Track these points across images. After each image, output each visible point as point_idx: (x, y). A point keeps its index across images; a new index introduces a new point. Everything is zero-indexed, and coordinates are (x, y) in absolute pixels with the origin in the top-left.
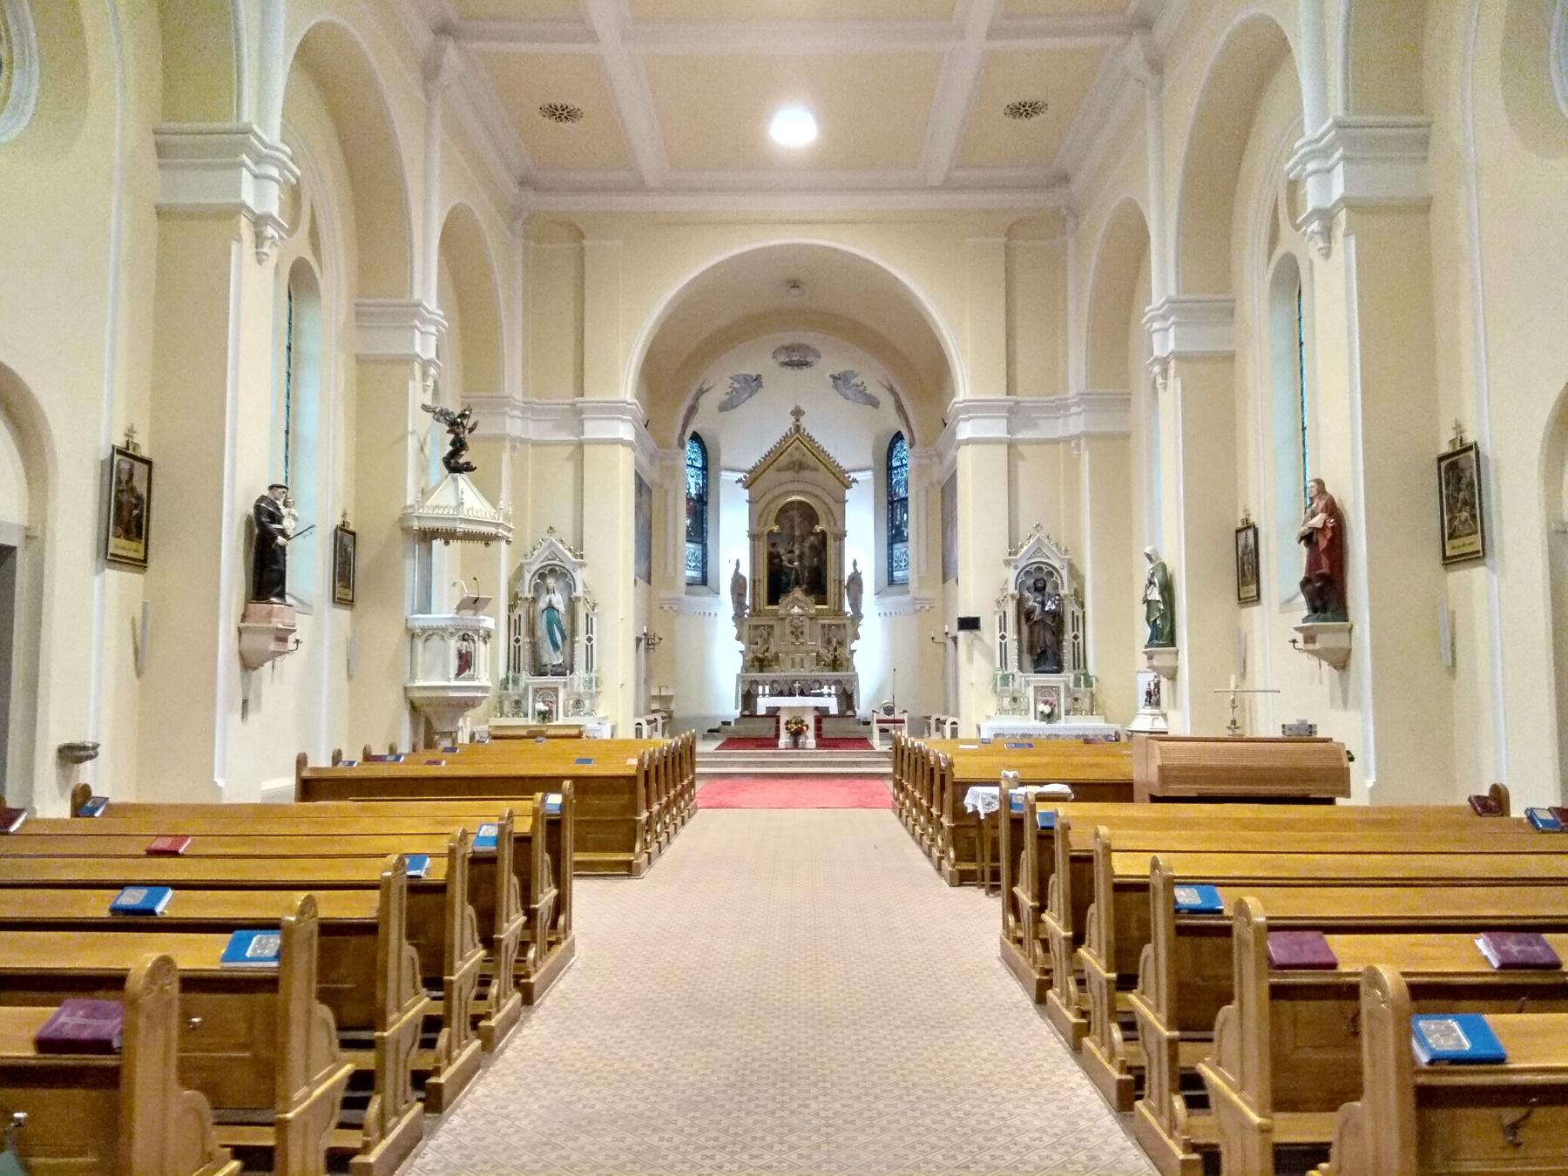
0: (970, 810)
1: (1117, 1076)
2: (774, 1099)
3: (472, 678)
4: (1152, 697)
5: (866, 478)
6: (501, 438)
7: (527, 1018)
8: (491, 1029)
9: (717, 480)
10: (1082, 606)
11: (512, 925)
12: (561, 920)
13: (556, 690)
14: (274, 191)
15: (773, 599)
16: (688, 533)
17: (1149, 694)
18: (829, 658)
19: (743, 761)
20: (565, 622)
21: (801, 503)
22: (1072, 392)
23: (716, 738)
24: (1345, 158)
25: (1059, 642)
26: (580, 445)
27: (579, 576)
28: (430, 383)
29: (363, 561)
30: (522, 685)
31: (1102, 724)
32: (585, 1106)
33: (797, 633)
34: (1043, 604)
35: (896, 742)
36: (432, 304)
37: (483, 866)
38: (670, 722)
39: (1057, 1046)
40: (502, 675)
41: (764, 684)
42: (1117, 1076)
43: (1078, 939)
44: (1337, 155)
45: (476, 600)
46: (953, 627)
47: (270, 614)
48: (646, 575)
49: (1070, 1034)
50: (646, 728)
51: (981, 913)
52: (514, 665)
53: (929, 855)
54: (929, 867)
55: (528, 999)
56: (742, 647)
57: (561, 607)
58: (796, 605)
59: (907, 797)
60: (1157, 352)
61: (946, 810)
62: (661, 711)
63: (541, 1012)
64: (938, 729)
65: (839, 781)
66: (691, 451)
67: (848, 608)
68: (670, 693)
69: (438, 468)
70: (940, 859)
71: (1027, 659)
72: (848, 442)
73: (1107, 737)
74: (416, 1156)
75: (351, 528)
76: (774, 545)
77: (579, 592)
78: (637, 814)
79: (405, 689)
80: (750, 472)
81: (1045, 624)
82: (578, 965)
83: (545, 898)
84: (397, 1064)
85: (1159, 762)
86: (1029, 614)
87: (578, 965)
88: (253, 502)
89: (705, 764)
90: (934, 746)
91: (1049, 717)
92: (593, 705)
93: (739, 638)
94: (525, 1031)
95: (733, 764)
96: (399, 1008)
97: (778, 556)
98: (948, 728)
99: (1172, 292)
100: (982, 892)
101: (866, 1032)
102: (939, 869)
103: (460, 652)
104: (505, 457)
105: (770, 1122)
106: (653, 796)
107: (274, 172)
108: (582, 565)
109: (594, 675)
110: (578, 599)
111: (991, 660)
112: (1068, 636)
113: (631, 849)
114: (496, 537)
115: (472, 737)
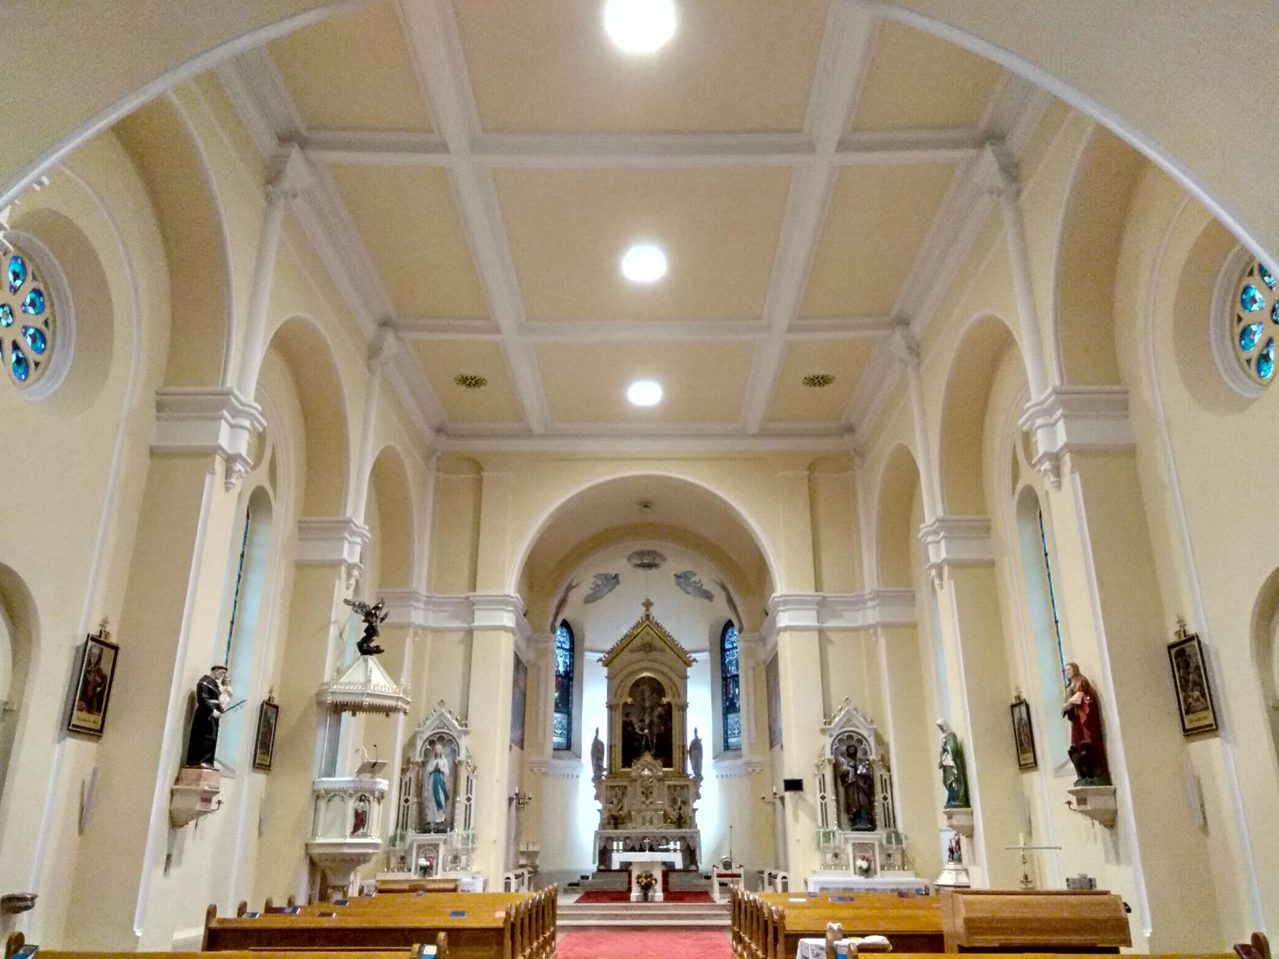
3: (365, 835)
5: (703, 657)
6: (404, 627)
10: (889, 770)
13: (436, 846)
15: (627, 762)
16: (557, 705)
17: (951, 851)
18: (674, 815)
19: (598, 914)
20: (449, 786)
21: (650, 678)
26: (470, 632)
27: (464, 743)
28: (353, 582)
30: (408, 842)
33: (647, 793)
34: (855, 768)
35: (734, 894)
36: (360, 520)
38: (535, 877)
40: (391, 832)
41: (618, 840)
47: (199, 778)
48: (520, 742)
50: (513, 882)
52: (402, 824)
58: (647, 767)
60: (933, 559)
66: (561, 636)
67: (690, 771)
68: (535, 848)
69: (353, 650)
71: (845, 818)
72: (689, 627)
73: (918, 891)
76: (628, 715)
77: (462, 756)
80: (609, 653)
81: (858, 787)
86: (844, 776)
90: (767, 898)
91: (866, 872)
92: (468, 861)
93: (597, 798)
97: (631, 724)
98: (779, 881)
104: (409, 641)
106: (518, 948)
107: (247, 423)
108: (466, 733)
109: (470, 832)
110: (460, 762)
111: (815, 820)
112: (879, 797)
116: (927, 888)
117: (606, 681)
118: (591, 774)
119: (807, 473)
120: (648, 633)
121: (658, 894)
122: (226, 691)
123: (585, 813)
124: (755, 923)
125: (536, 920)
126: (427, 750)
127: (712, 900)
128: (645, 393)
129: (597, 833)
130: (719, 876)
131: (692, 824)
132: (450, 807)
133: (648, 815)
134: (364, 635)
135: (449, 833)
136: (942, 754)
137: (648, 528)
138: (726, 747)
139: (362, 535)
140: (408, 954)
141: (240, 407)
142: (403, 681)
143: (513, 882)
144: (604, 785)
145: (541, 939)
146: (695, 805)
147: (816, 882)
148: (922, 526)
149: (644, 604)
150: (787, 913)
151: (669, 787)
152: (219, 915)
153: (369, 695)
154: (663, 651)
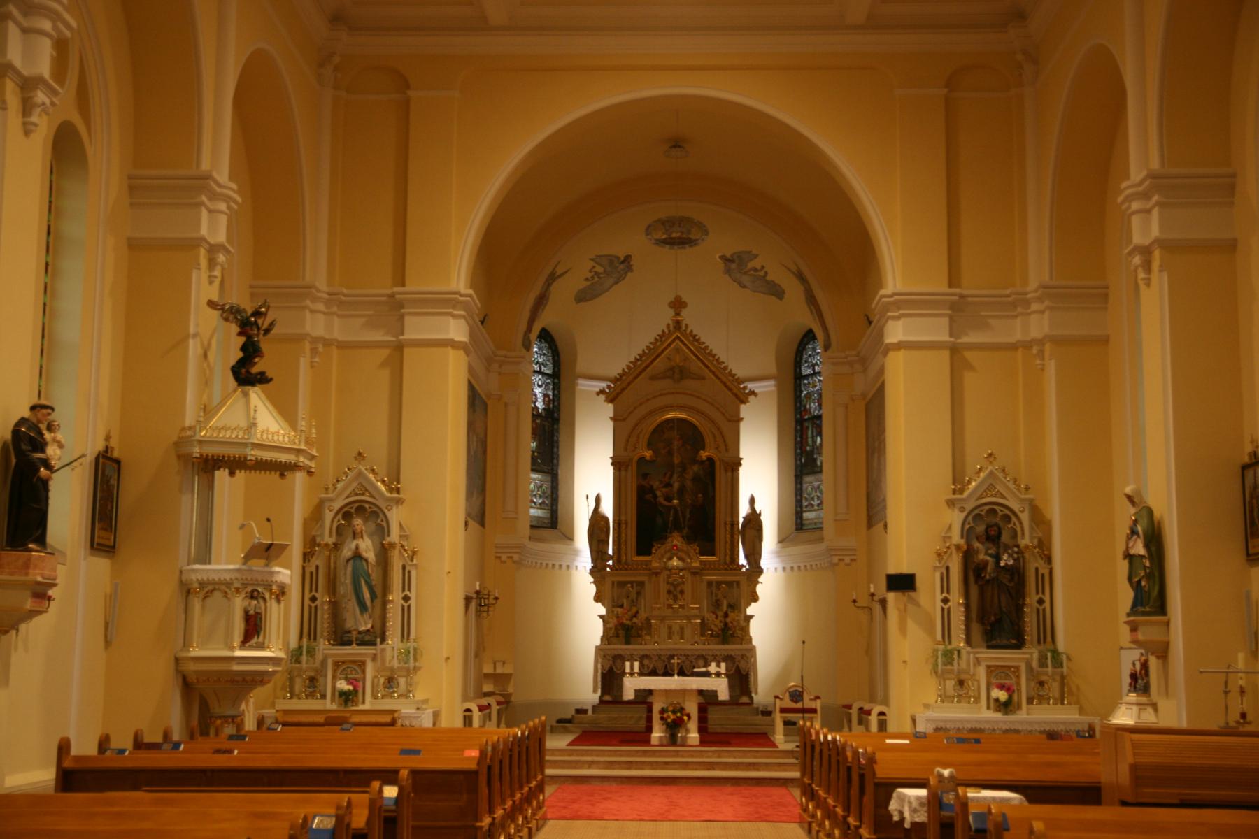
3: (261, 647)
4: (1139, 681)
6: (298, 339)
10: (1049, 560)
13: (362, 665)
14: (45, 49)
15: (644, 548)
16: (534, 460)
17: (1134, 676)
18: (716, 624)
19: (600, 762)
20: (375, 576)
21: (681, 420)
22: (1033, 284)
23: (567, 731)
24: (1159, 204)
25: (1019, 609)
26: (399, 348)
27: (395, 516)
28: (217, 272)
29: (130, 491)
30: (319, 657)
33: (675, 592)
34: (997, 558)
35: (804, 734)
36: (222, 175)
38: (507, 709)
40: (293, 644)
41: (632, 660)
44: (1156, 198)
47: (27, 566)
48: (479, 515)
52: (309, 630)
56: (603, 611)
57: (371, 556)
58: (675, 558)
61: (865, 819)
62: (494, 689)
64: (860, 722)
66: (537, 353)
67: (742, 560)
68: (507, 670)
72: (743, 341)
73: (1079, 734)
75: (116, 455)
76: (645, 476)
77: (394, 536)
78: (477, 818)
79: (177, 660)
80: (615, 380)
86: (981, 567)
88: (11, 427)
89: (556, 764)
90: (854, 740)
91: (1005, 707)
92: (409, 684)
93: (598, 598)
95: (590, 764)
97: (651, 490)
98: (873, 719)
103: (246, 613)
104: (304, 363)
106: (497, 799)
107: (47, 25)
108: (399, 502)
109: (411, 645)
110: (392, 545)
111: (931, 632)
112: (1031, 599)
114: (295, 467)
115: (260, 722)
116: (1091, 729)
117: (611, 424)
118: (589, 565)
120: (678, 350)
121: (694, 736)
122: (54, 440)
123: (584, 619)
124: (833, 775)
125: (513, 771)
129: (598, 649)
130: (783, 710)
132: (378, 612)
135: (380, 647)
136: (1129, 539)
137: (677, 183)
138: (798, 524)
139: (227, 199)
140: (366, 796)
142: (302, 424)
146: (749, 611)
148: (1124, 185)
150: (878, 756)
151: (710, 584)
152: (74, 751)
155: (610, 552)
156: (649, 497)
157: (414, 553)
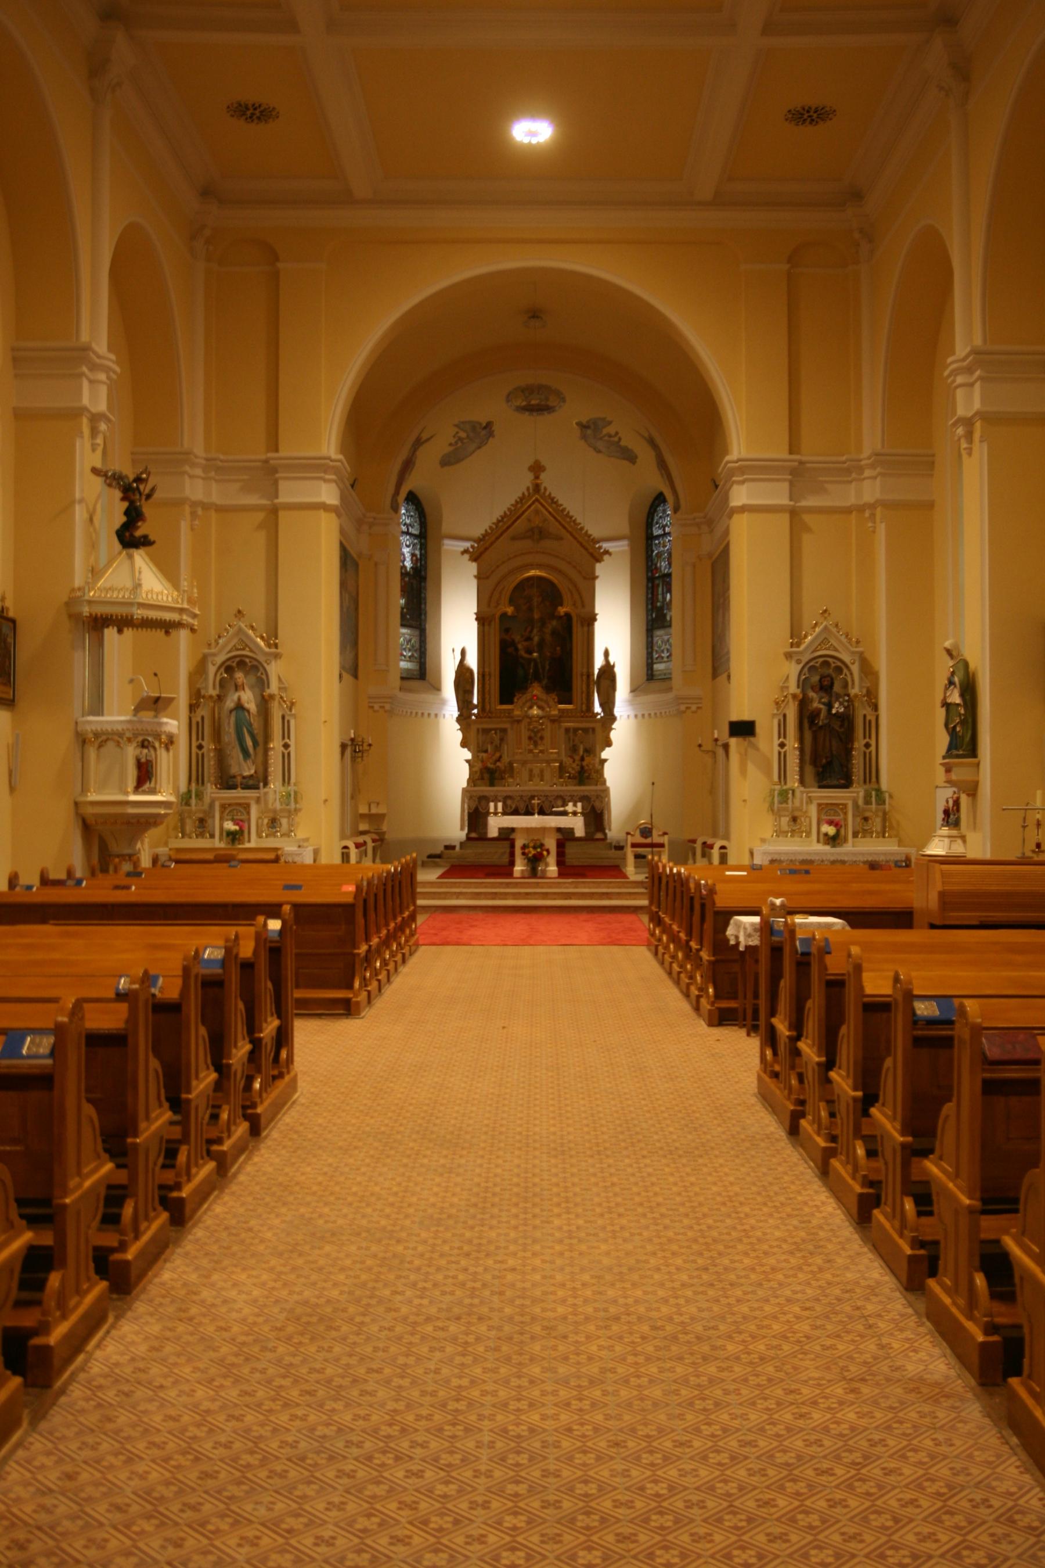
0: (732, 942)
1: (858, 1189)
2: (508, 1359)
3: (153, 791)
4: (951, 817)
5: (619, 548)
7: (256, 1148)
8: (224, 1153)
9: (438, 551)
10: (876, 707)
11: (240, 1052)
12: (284, 1054)
13: (247, 807)
15: (507, 696)
16: (403, 616)
17: (946, 812)
18: (573, 767)
19: (466, 893)
20: (257, 724)
22: (866, 452)
23: (437, 865)
25: (848, 752)
26: (274, 511)
27: (274, 670)
28: (99, 440)
30: (207, 800)
31: (895, 848)
32: (326, 1222)
33: (535, 738)
34: (830, 706)
35: (653, 867)
36: (101, 347)
37: (212, 986)
38: (382, 846)
39: (806, 1171)
40: (183, 788)
41: (495, 800)
42: (858, 1189)
43: (869, 1099)
44: (978, 373)
45: (157, 700)
46: (722, 732)
48: (352, 668)
49: (819, 1156)
50: (353, 852)
51: (740, 1052)
52: (196, 775)
53: (687, 995)
54: (686, 1007)
55: (256, 1130)
57: (252, 707)
58: (535, 707)
59: (663, 932)
60: (961, 412)
61: (706, 943)
62: (369, 829)
63: (269, 1142)
64: (704, 855)
65: (584, 916)
67: (597, 709)
68: (382, 810)
69: (108, 542)
70: (698, 997)
71: (809, 770)
73: (897, 864)
74: (165, 1261)
76: (507, 631)
77: (274, 688)
78: (355, 946)
79: (76, 804)
80: (479, 541)
82: (303, 1100)
83: (270, 1027)
84: (147, 1172)
85: (939, 887)
86: (814, 716)
87: (303, 1100)
90: (697, 873)
91: (833, 840)
92: (290, 825)
93: (464, 744)
94: (256, 1159)
95: (458, 895)
96: (147, 1117)
97: (513, 644)
98: (715, 853)
99: (978, 341)
100: (743, 1032)
101: (611, 1161)
102: (697, 1009)
104: (184, 526)
105: (513, 1234)
108: (277, 656)
109: (291, 788)
110: (272, 697)
111: (768, 773)
112: (859, 744)
113: (350, 986)
114: (179, 625)
115: (155, 860)
117: (475, 582)
119: (787, 267)
120: (537, 512)
121: (553, 869)
126: (222, 680)
127: (625, 877)
128: (532, 132)
129: (465, 791)
130: (634, 845)
131: (600, 779)
133: (537, 767)
134: (124, 519)
135: (262, 790)
136: (946, 689)
137: (541, 353)
138: (649, 675)
139: (107, 370)
141: (98, 361)
142: (185, 584)
143: (353, 852)
144: (474, 728)
145: (399, 919)
146: (604, 755)
147: (765, 853)
148: (949, 360)
149: (531, 469)
150: (718, 887)
151: (567, 730)
153: (141, 605)
154: (560, 538)
155: (475, 701)
156: (510, 650)
157: (293, 704)
